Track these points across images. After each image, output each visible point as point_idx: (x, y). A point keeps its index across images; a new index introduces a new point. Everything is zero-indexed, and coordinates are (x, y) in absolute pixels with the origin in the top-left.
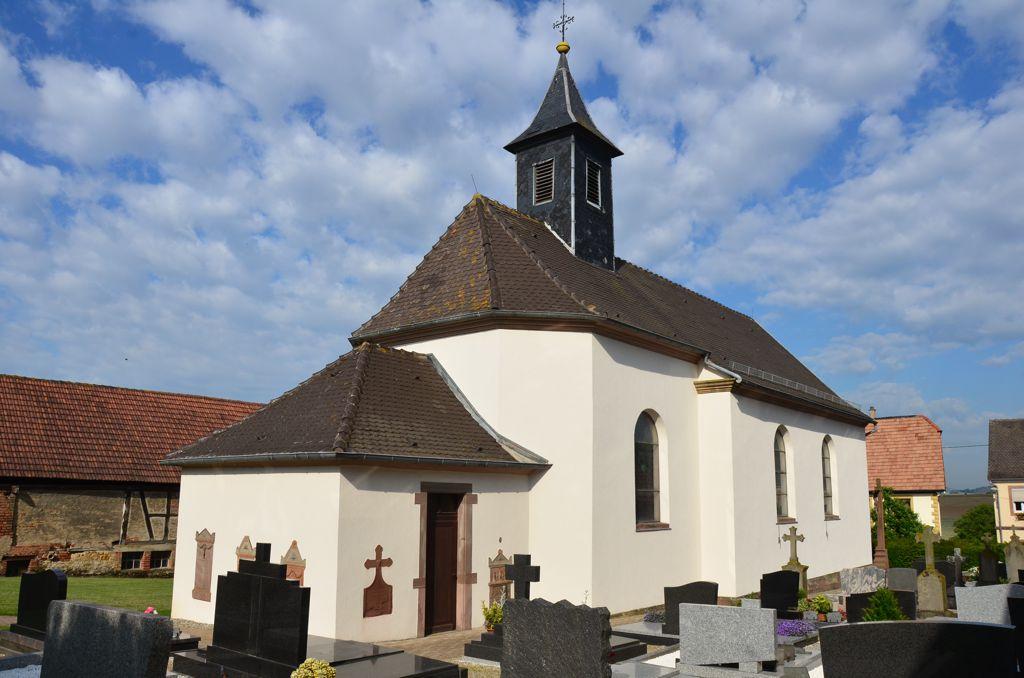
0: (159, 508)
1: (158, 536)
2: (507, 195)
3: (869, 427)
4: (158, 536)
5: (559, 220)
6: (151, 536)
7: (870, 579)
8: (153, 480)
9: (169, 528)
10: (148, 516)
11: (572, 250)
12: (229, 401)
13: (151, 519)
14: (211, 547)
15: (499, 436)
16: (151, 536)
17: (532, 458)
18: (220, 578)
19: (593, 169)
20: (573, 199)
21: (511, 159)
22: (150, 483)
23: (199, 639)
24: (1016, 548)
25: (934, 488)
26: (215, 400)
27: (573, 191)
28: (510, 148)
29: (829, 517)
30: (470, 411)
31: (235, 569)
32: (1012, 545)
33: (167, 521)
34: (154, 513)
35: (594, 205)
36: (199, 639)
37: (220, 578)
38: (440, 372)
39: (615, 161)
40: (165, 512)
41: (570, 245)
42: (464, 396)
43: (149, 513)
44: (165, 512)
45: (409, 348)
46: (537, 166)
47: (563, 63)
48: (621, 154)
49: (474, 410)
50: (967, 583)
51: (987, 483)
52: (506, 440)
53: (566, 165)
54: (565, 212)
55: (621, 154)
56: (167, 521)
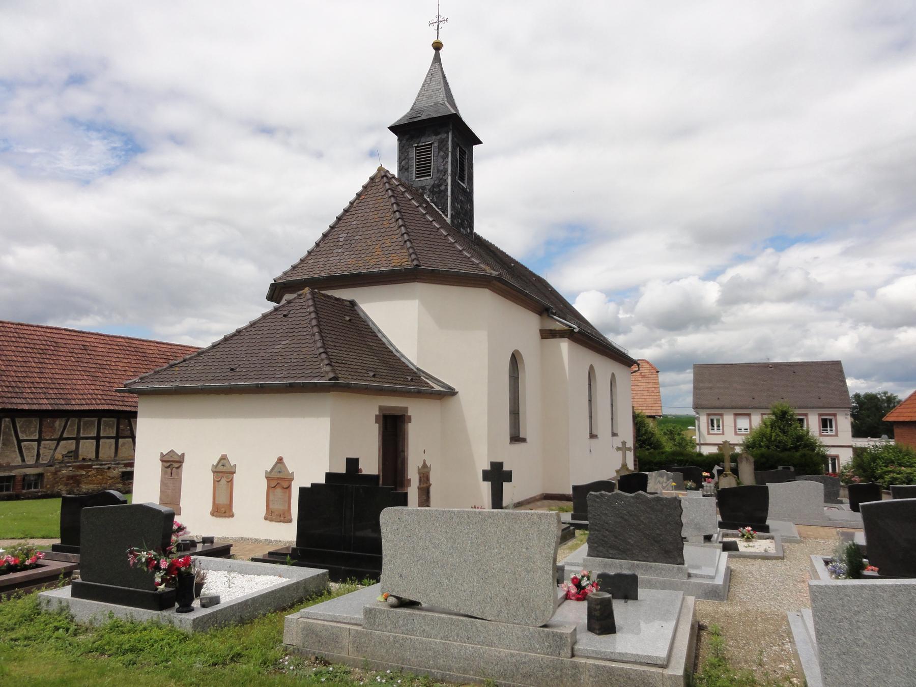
0: (32, 433)
1: (30, 460)
2: (393, 170)
3: (635, 367)
4: (30, 460)
5: (437, 195)
6: (23, 460)
7: (661, 480)
8: (26, 407)
9: (41, 452)
10: (19, 442)
11: (448, 220)
12: (89, 333)
13: (23, 444)
14: (179, 467)
15: (418, 369)
16: (23, 460)
17: (443, 387)
18: (302, 490)
19: (462, 153)
20: (450, 178)
21: (394, 138)
22: (23, 410)
23: (231, 545)
24: (746, 457)
25: (654, 414)
26: (75, 331)
27: (449, 171)
28: (393, 129)
29: (593, 436)
30: (391, 348)
31: (322, 481)
32: (743, 456)
33: (39, 445)
34: (26, 438)
35: (461, 183)
36: (231, 545)
37: (302, 490)
38: (362, 314)
39: (476, 148)
40: (37, 437)
41: (447, 216)
42: (384, 336)
43: (21, 438)
44: (37, 437)
45: (329, 293)
46: (416, 147)
47: (437, 59)
48: (481, 143)
49: (394, 347)
50: (570, 492)
51: (692, 412)
52: (424, 372)
53: (444, 149)
54: (443, 188)
55: (481, 143)
56: (39, 445)
